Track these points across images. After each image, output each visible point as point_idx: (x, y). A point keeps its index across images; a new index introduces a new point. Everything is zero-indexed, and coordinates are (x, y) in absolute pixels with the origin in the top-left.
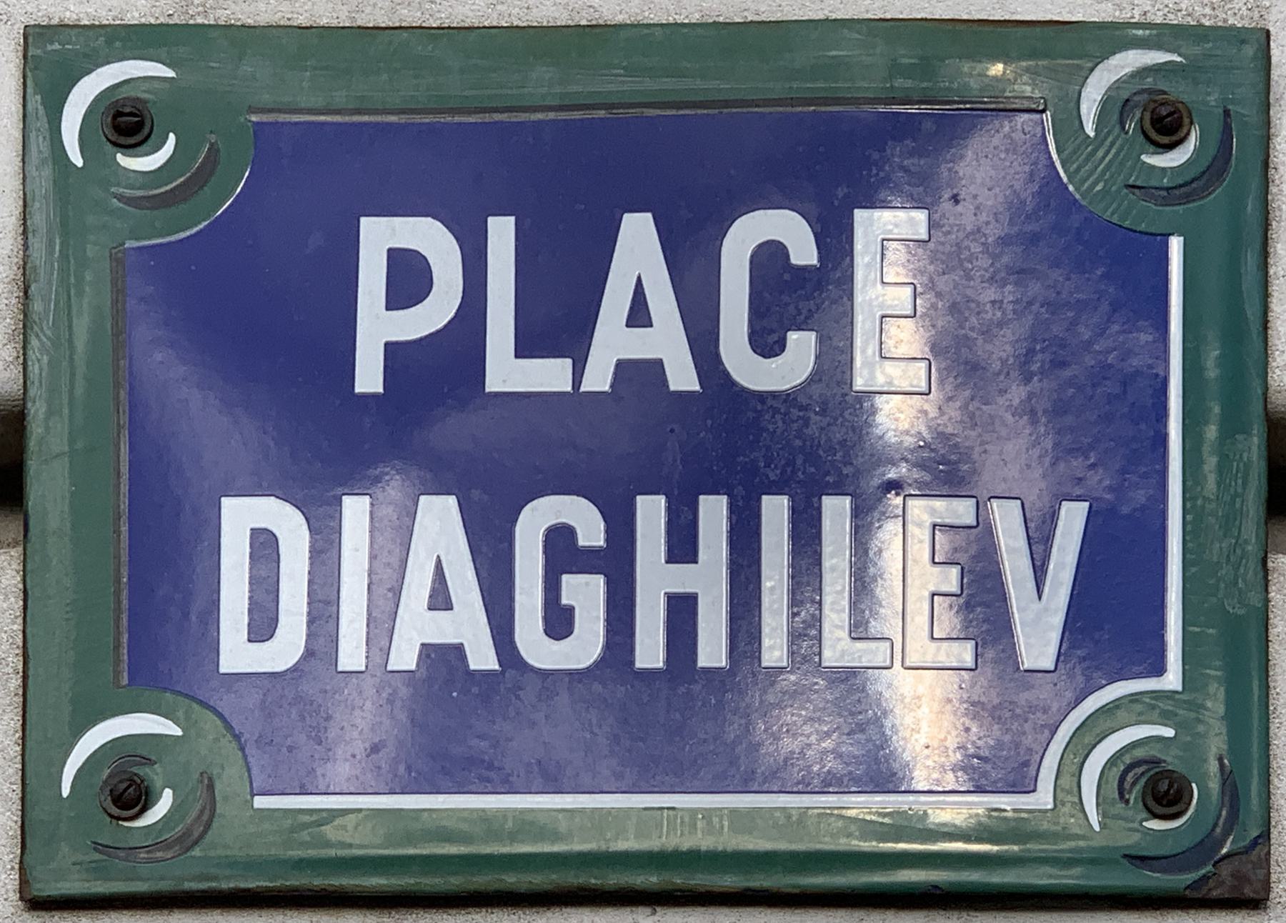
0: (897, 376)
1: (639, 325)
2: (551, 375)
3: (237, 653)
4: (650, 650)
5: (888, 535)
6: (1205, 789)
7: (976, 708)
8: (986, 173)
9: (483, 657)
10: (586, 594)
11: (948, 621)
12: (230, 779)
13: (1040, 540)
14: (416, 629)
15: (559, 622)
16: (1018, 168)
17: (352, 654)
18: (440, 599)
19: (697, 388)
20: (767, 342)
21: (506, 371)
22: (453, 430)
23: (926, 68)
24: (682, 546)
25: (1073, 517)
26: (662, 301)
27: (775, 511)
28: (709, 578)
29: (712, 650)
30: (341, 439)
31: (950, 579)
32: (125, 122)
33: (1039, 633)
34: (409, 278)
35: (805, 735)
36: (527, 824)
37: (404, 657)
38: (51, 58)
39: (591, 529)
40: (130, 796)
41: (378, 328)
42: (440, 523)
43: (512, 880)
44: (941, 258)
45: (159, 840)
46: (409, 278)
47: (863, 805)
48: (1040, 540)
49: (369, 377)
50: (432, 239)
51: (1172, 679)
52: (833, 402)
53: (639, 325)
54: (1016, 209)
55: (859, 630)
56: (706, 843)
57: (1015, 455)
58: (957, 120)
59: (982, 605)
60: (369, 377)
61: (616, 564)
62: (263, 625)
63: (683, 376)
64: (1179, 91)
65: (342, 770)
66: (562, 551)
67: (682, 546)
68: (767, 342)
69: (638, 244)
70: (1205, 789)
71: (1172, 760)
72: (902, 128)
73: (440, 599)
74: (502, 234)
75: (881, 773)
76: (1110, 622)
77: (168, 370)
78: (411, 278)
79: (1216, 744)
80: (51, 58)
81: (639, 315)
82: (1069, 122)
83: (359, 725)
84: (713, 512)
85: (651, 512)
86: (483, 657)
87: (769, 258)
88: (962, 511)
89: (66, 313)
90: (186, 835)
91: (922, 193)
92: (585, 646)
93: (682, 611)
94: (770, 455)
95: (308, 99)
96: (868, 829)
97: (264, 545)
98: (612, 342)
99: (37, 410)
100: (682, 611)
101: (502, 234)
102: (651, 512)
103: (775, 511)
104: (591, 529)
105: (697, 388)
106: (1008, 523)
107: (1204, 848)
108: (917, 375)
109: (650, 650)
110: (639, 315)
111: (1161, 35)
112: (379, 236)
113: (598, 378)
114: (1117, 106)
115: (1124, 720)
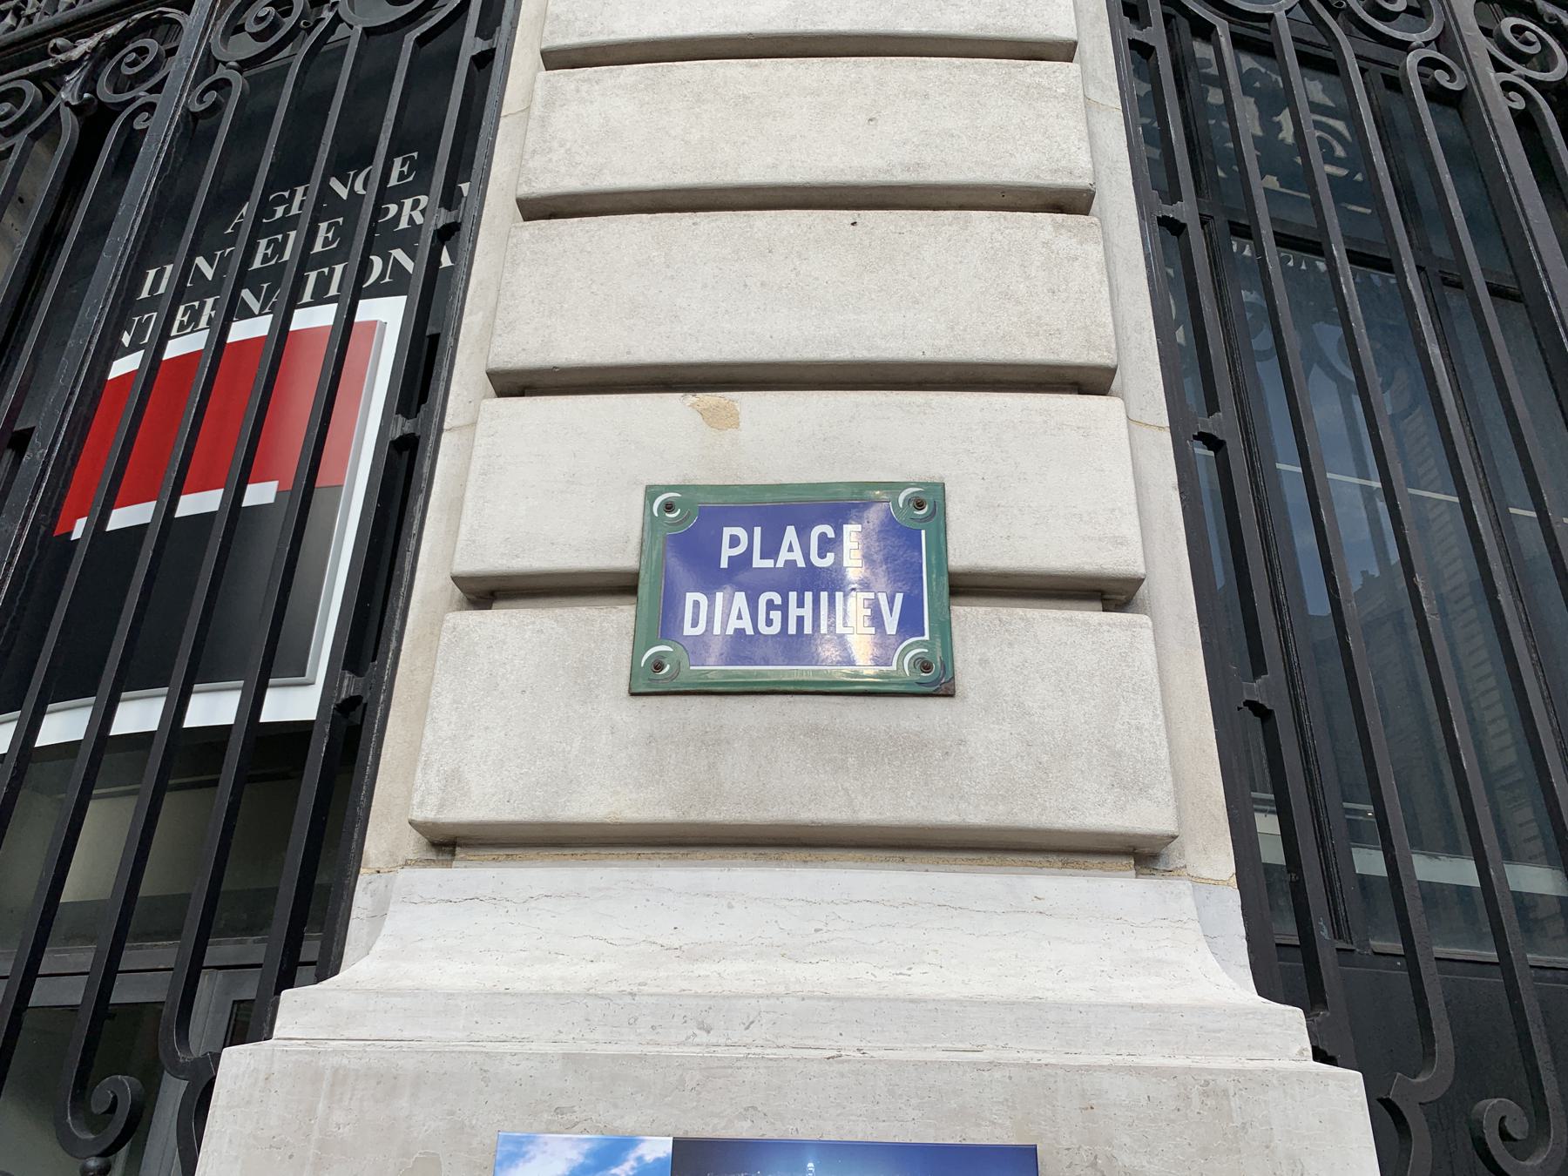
0: (853, 562)
1: (791, 551)
2: (769, 563)
3: (688, 630)
4: (792, 630)
5: (851, 600)
6: (937, 666)
7: (876, 644)
8: (874, 515)
9: (750, 631)
10: (776, 616)
11: (867, 623)
12: (685, 662)
13: (891, 602)
14: (734, 624)
15: (769, 622)
16: (882, 515)
17: (717, 630)
18: (740, 617)
19: (262, 720)
20: (822, 555)
21: (757, 562)
22: (743, 577)
23: (861, 492)
24: (801, 604)
25: (899, 597)
26: (796, 546)
27: (824, 595)
28: (807, 612)
29: (808, 630)
30: (712, 578)
31: (869, 612)
32: (669, 507)
33: (891, 625)
34: (735, 541)
35: (828, 651)
36: (759, 673)
37: (730, 631)
38: (651, 492)
39: (778, 600)
40: (658, 667)
41: (727, 553)
42: (740, 599)
43: (755, 688)
44: (865, 535)
45: (665, 678)
46: (735, 541)
47: (847, 669)
48: (891, 602)
49: (724, 564)
50: (741, 532)
51: (927, 637)
52: (838, 567)
53: (791, 551)
54: (882, 524)
55: (845, 625)
56: (805, 678)
57: (882, 581)
58: (867, 504)
59: (877, 619)
60: (724, 564)
61: (784, 608)
62: (695, 624)
63: (801, 564)
64: (923, 497)
65: (712, 659)
66: (770, 605)
67: (801, 604)
68: (822, 555)
69: (791, 533)
70: (937, 666)
71: (927, 658)
72: (855, 506)
73: (740, 617)
74: (757, 531)
75: (851, 662)
76: (910, 622)
77: (673, 562)
78: (734, 541)
79: (939, 654)
80: (651, 492)
81: (791, 549)
82: (896, 504)
83: (716, 648)
84: (808, 596)
85: (793, 596)
86: (750, 631)
87: (823, 536)
88: (871, 596)
89: (651, 550)
90: (673, 676)
91: (859, 521)
92: (776, 629)
93: (800, 620)
94: (818, 582)
95: (712, 501)
96: (848, 675)
97: (696, 604)
98: (784, 555)
99: (642, 573)
100: (800, 620)
101: (757, 531)
102: (793, 596)
103: (824, 595)
104: (778, 600)
105: (262, 720)
106: (883, 599)
107: (937, 681)
108: (859, 563)
109: (792, 630)
110: (791, 549)
111: (918, 485)
112: (727, 532)
113: (780, 564)
114: (908, 500)
115: (913, 648)
